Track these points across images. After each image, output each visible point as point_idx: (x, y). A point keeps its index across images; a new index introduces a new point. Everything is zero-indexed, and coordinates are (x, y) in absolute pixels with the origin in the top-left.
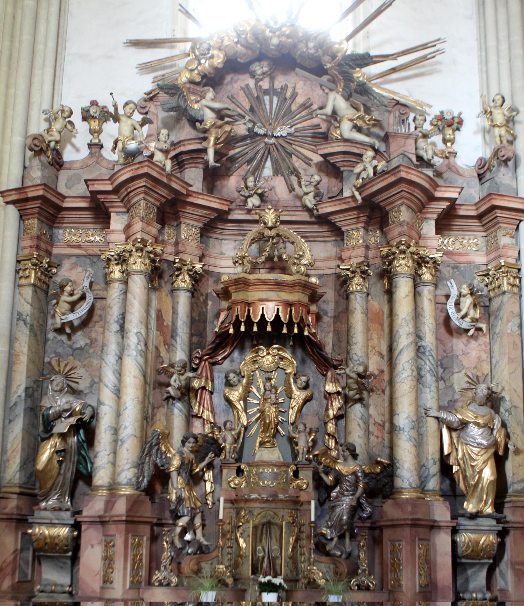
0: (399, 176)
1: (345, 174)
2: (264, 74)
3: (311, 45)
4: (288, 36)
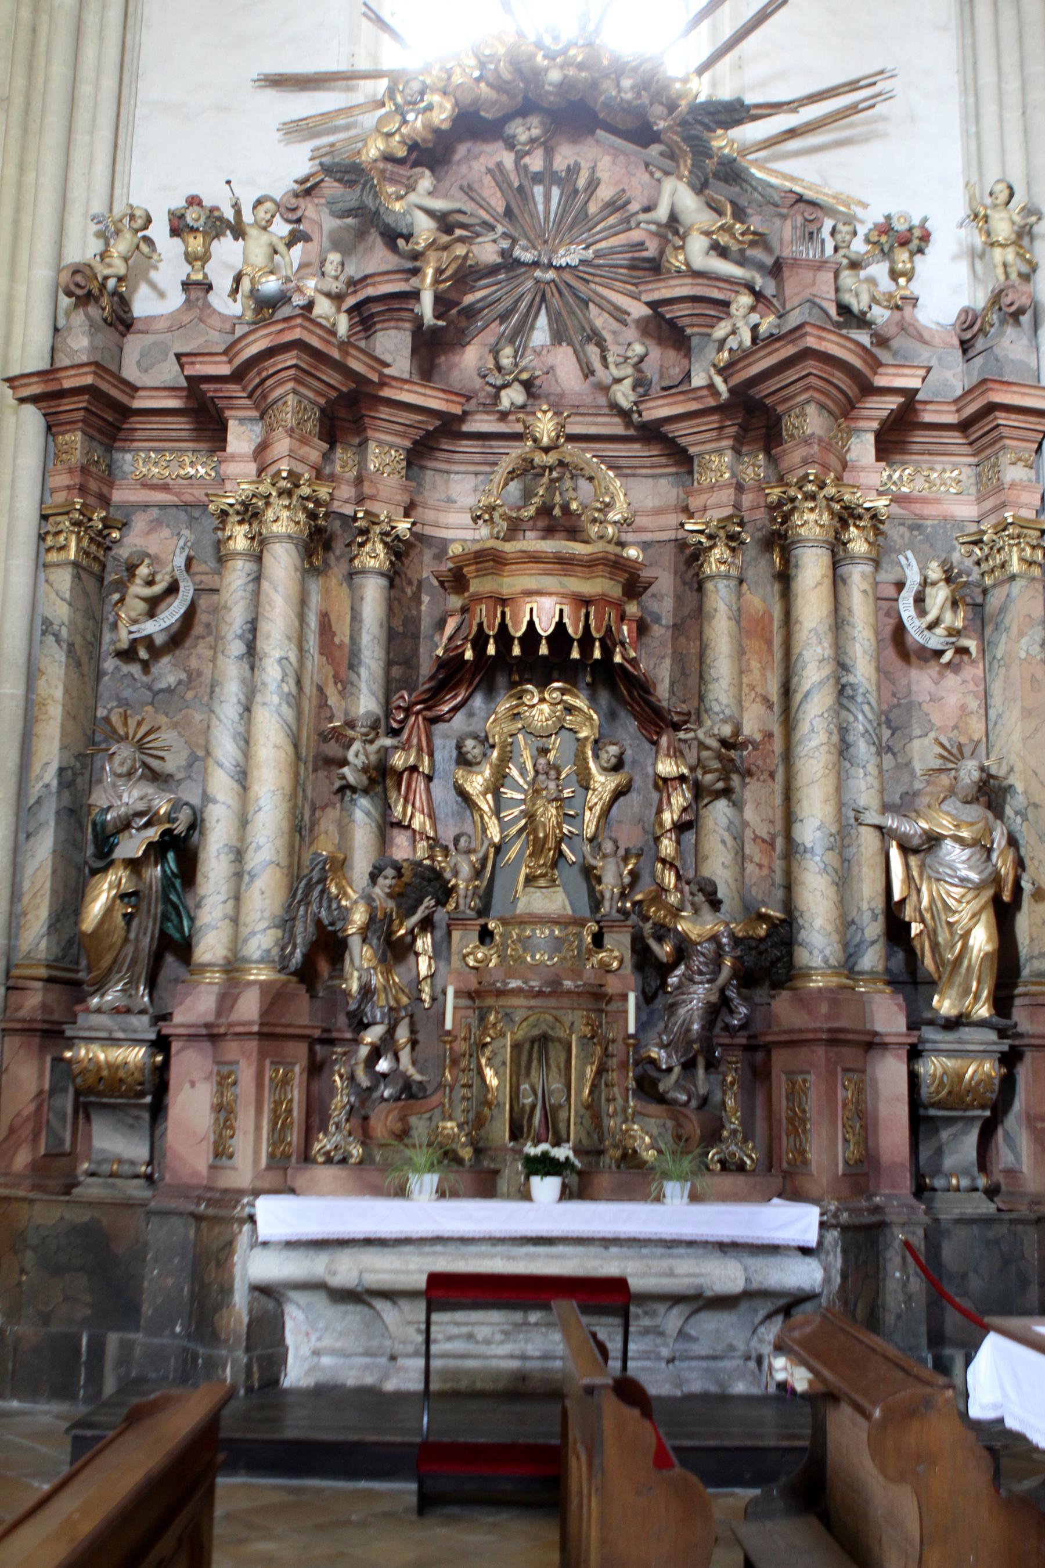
0: (802, 345)
1: (695, 341)
2: (532, 141)
3: (627, 83)
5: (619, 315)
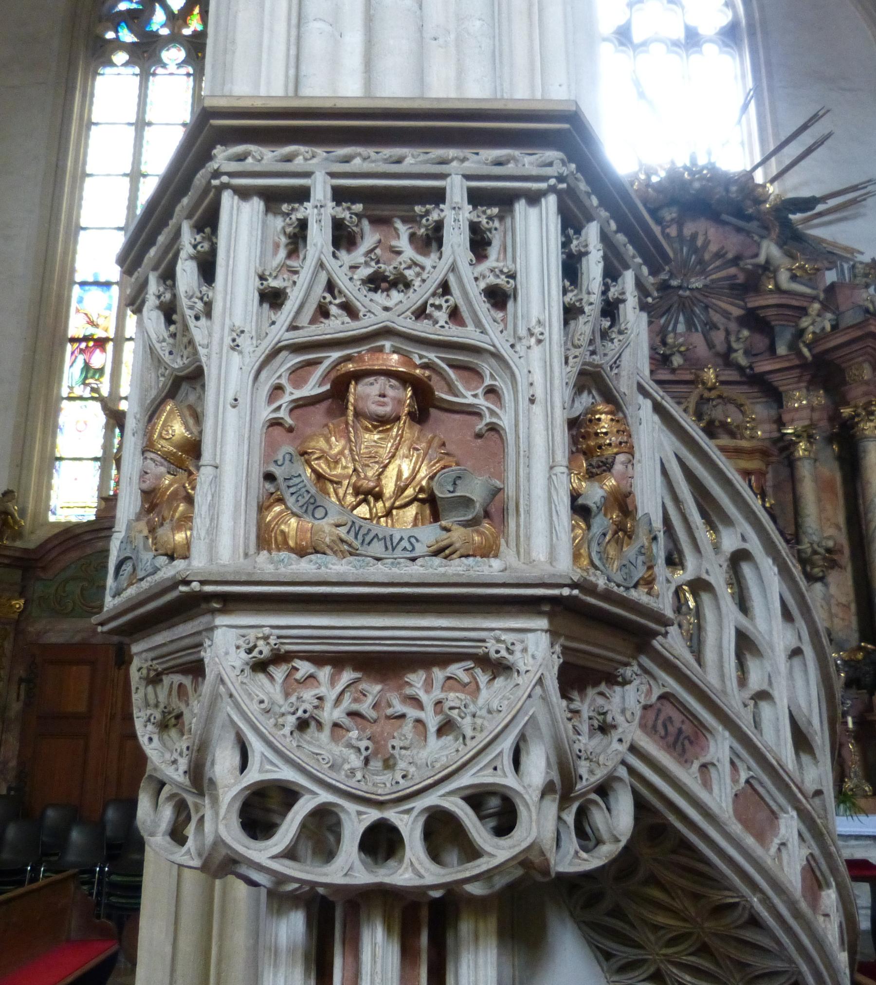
0: (867, 330)
1: (777, 329)
2: (672, 220)
3: (734, 188)
4: (709, 180)
5: (726, 314)
